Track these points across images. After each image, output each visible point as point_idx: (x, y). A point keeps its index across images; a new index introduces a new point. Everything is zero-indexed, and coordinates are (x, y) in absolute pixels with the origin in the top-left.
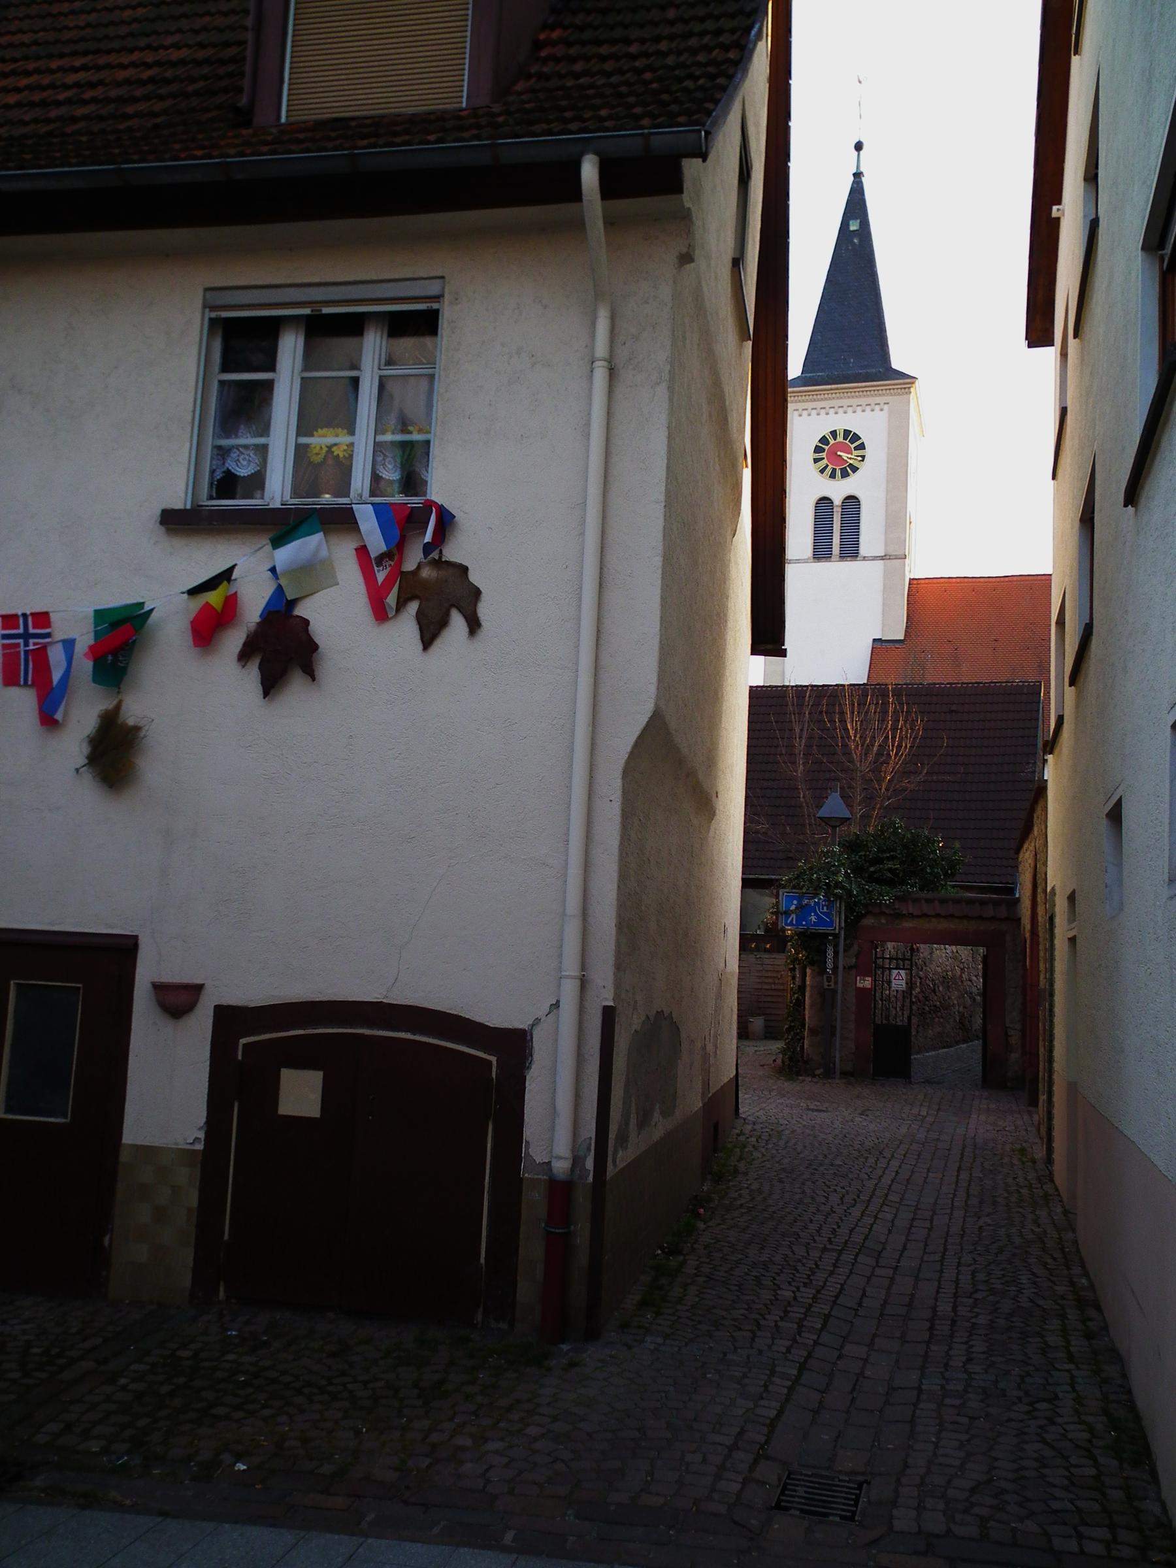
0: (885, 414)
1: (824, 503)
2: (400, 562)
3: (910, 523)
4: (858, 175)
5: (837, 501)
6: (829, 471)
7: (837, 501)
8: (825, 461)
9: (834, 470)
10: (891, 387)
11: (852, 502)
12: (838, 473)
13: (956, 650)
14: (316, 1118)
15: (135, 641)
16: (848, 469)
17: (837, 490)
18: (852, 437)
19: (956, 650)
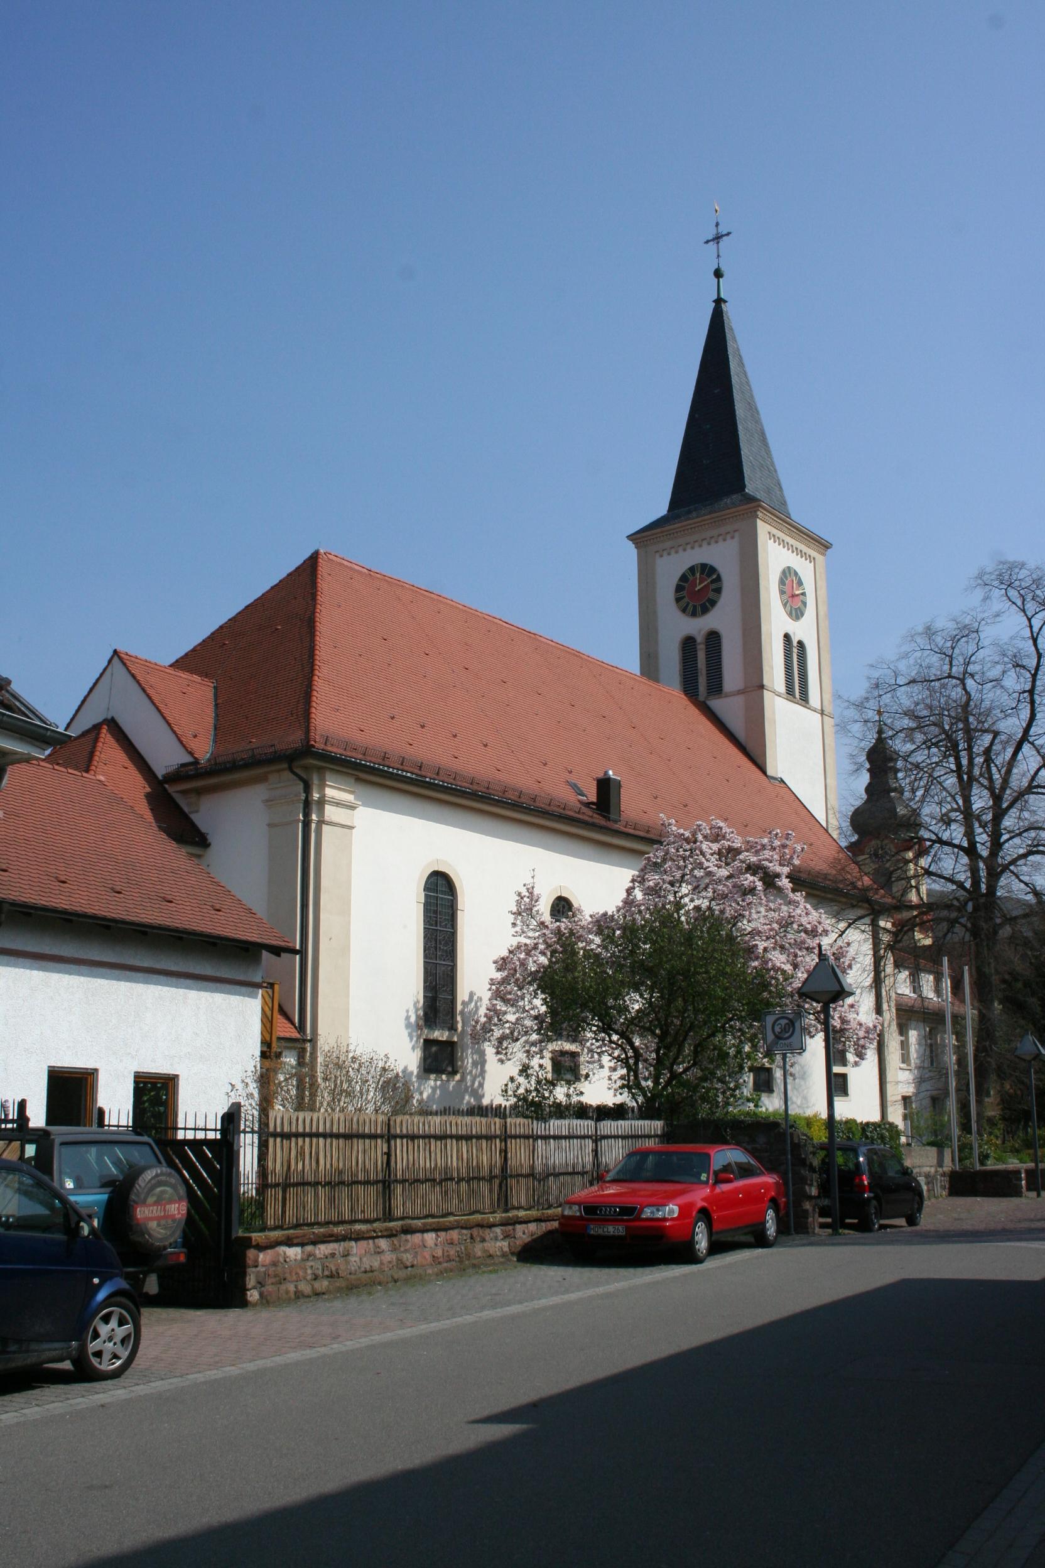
0: (736, 539)
1: (688, 644)
2: (981, 857)
3: (137, 658)
4: (719, 301)
5: (700, 639)
6: (690, 608)
7: (700, 639)
8: (686, 600)
9: (695, 607)
10: (728, 516)
11: (714, 639)
12: (699, 609)
13: (669, 760)
14: (145, 1307)
15: (411, 1040)
16: (707, 604)
17: (698, 626)
18: (708, 570)
19: (669, 760)
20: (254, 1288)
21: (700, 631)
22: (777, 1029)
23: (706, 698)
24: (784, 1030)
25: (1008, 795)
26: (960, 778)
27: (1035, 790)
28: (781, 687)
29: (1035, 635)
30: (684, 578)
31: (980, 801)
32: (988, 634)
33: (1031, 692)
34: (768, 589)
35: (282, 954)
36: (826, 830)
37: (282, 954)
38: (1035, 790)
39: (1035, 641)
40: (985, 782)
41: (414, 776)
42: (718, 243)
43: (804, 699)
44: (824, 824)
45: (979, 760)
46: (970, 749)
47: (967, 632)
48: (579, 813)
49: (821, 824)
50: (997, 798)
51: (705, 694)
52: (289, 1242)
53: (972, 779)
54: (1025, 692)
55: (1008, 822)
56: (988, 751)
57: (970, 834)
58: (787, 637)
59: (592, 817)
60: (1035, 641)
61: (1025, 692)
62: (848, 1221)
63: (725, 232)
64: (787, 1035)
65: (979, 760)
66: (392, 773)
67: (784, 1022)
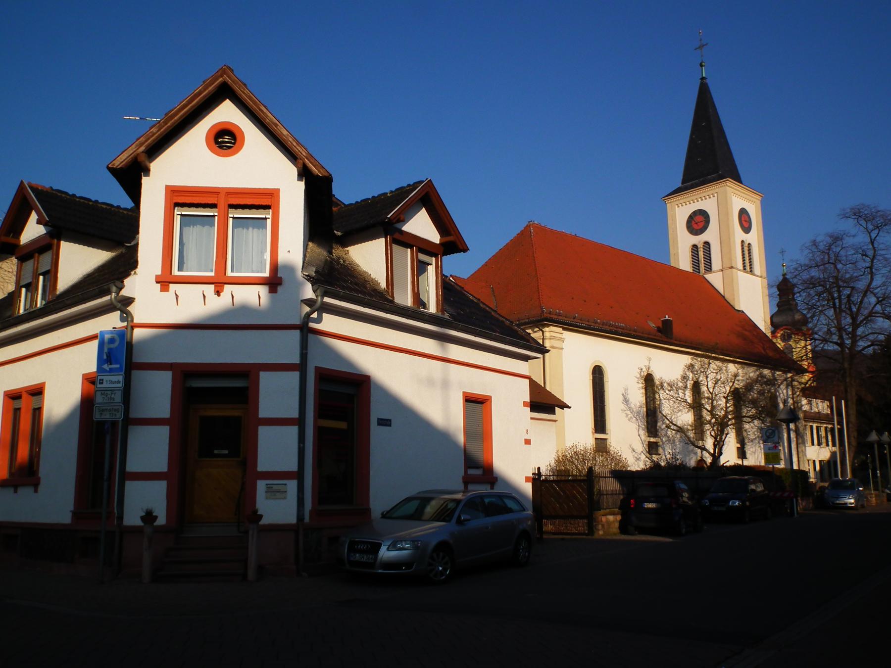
1: (695, 248)
5: (700, 246)
11: (707, 244)
17: (699, 240)
20: (601, 529)
21: (699, 242)
22: (768, 434)
23: (704, 274)
24: (771, 434)
25: (861, 318)
26: (835, 311)
27: (874, 315)
28: (741, 267)
29: (872, 241)
30: (690, 217)
31: (847, 320)
32: (848, 241)
33: (871, 268)
34: (733, 221)
35: (564, 409)
36: (724, 297)
37: (564, 409)
38: (874, 315)
39: (872, 243)
40: (849, 312)
41: (586, 326)
42: (701, 49)
43: (751, 271)
44: (722, 293)
45: (844, 301)
46: (840, 297)
47: (836, 239)
48: (655, 336)
49: (720, 293)
50: (854, 319)
51: (704, 272)
52: (611, 514)
53: (841, 311)
54: (867, 268)
55: (860, 331)
56: (849, 296)
57: (841, 337)
58: (743, 241)
59: (661, 337)
60: (872, 243)
61: (867, 268)
62: (216, 452)
63: (705, 43)
64: (772, 436)
65: (844, 301)
66: (583, 326)
67: (770, 431)
